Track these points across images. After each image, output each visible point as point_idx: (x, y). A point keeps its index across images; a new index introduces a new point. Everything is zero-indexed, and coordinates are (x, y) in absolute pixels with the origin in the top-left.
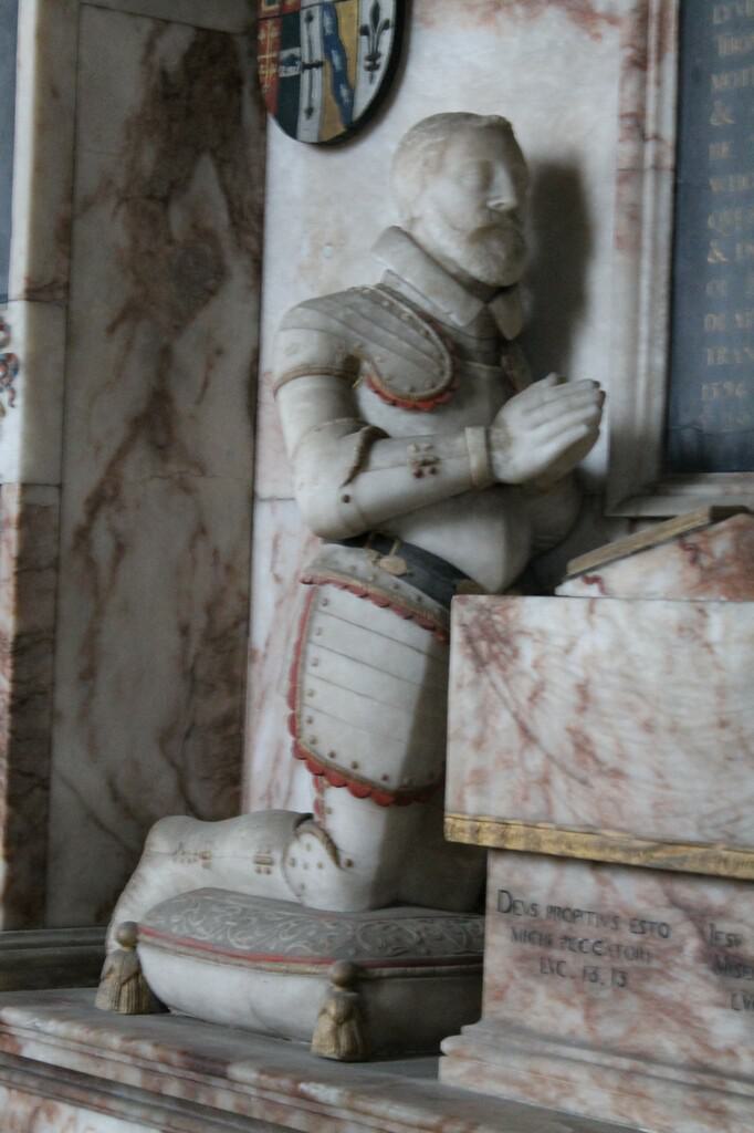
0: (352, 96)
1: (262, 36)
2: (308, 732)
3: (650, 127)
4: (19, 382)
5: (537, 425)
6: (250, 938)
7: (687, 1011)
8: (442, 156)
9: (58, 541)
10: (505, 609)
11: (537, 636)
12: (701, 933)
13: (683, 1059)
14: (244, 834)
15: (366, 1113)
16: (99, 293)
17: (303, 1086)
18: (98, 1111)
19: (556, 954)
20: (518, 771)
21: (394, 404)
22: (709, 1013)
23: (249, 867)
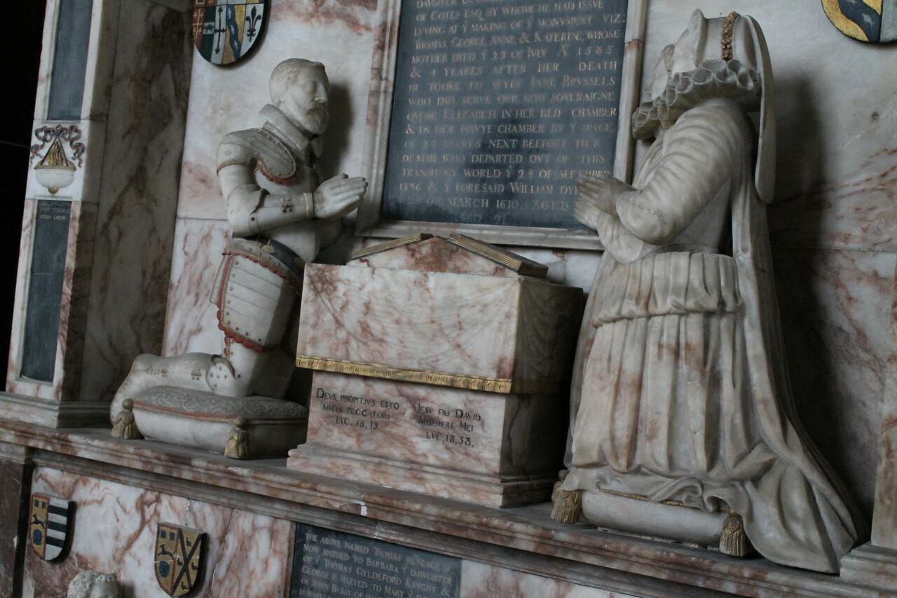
0: (240, 46)
1: (195, 15)
2: (226, 319)
3: (384, 75)
4: (84, 156)
5: (337, 194)
6: (194, 406)
7: (405, 438)
8: (296, 77)
9: (96, 229)
10: (331, 270)
11: (346, 282)
12: (414, 407)
13: (402, 458)
14: (186, 362)
15: (262, 480)
16: (120, 119)
17: (230, 468)
18: (112, 481)
19: (344, 415)
20: (334, 339)
21: (272, 180)
22: (415, 439)
23: (189, 377)
